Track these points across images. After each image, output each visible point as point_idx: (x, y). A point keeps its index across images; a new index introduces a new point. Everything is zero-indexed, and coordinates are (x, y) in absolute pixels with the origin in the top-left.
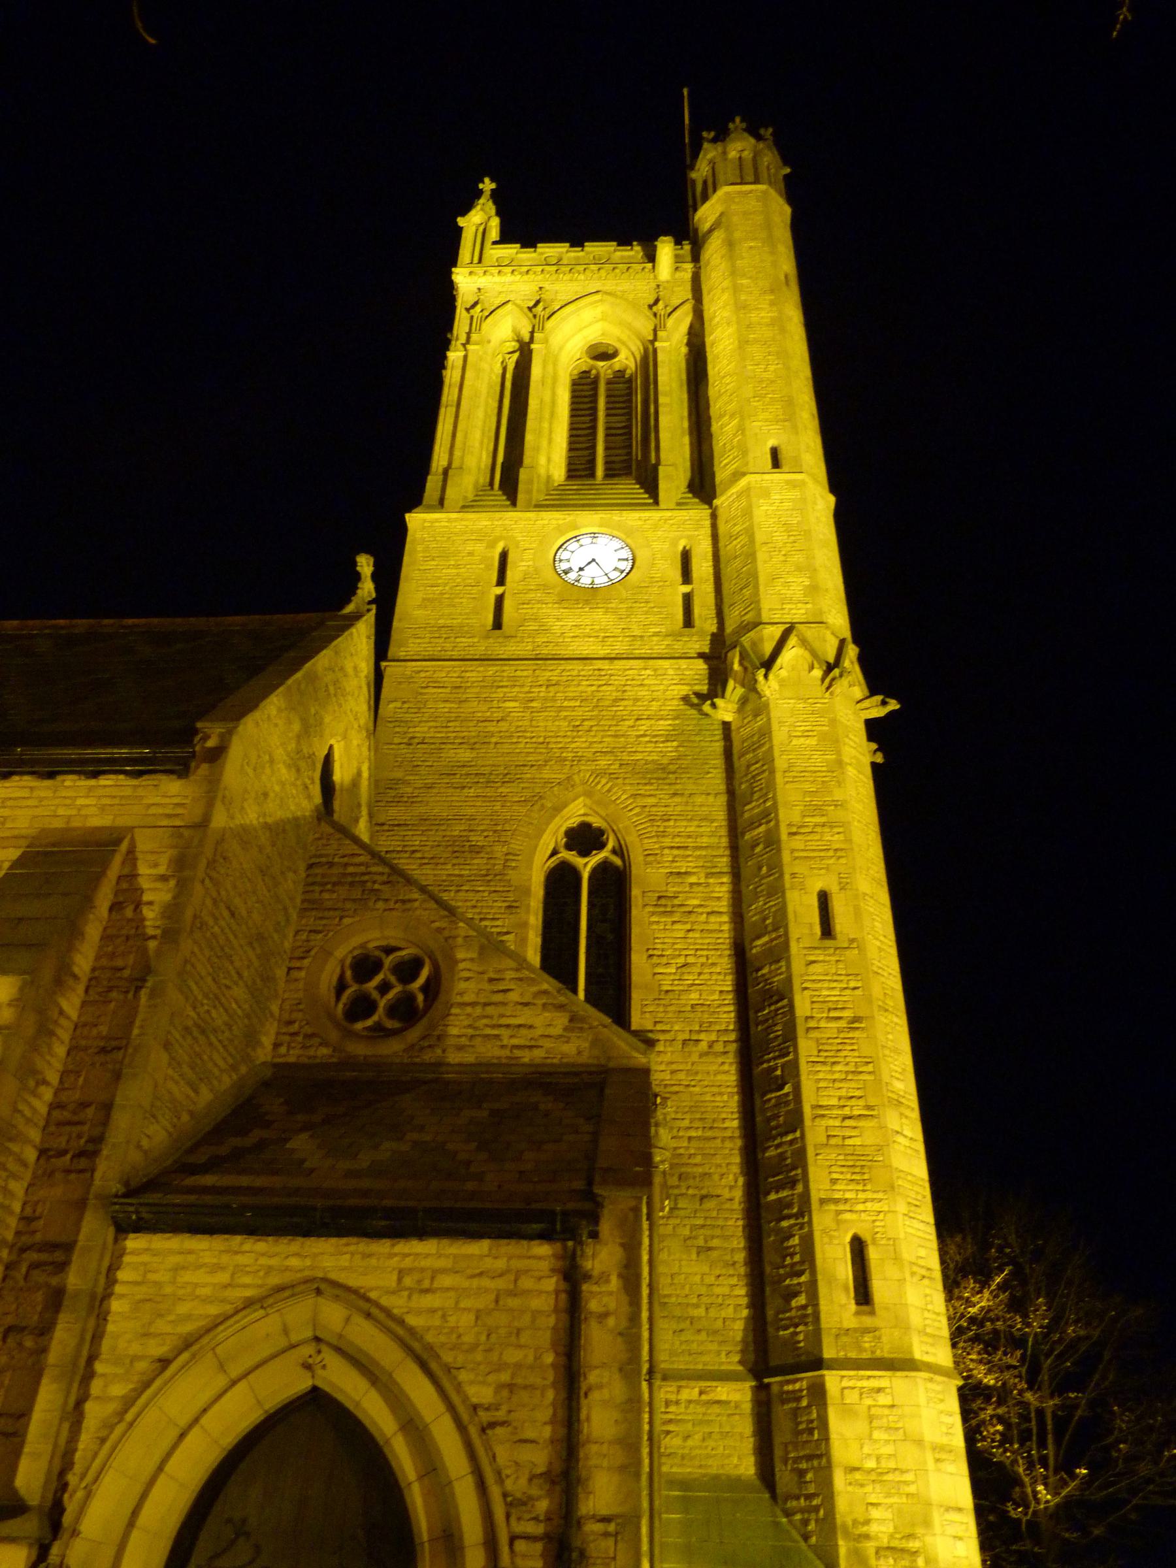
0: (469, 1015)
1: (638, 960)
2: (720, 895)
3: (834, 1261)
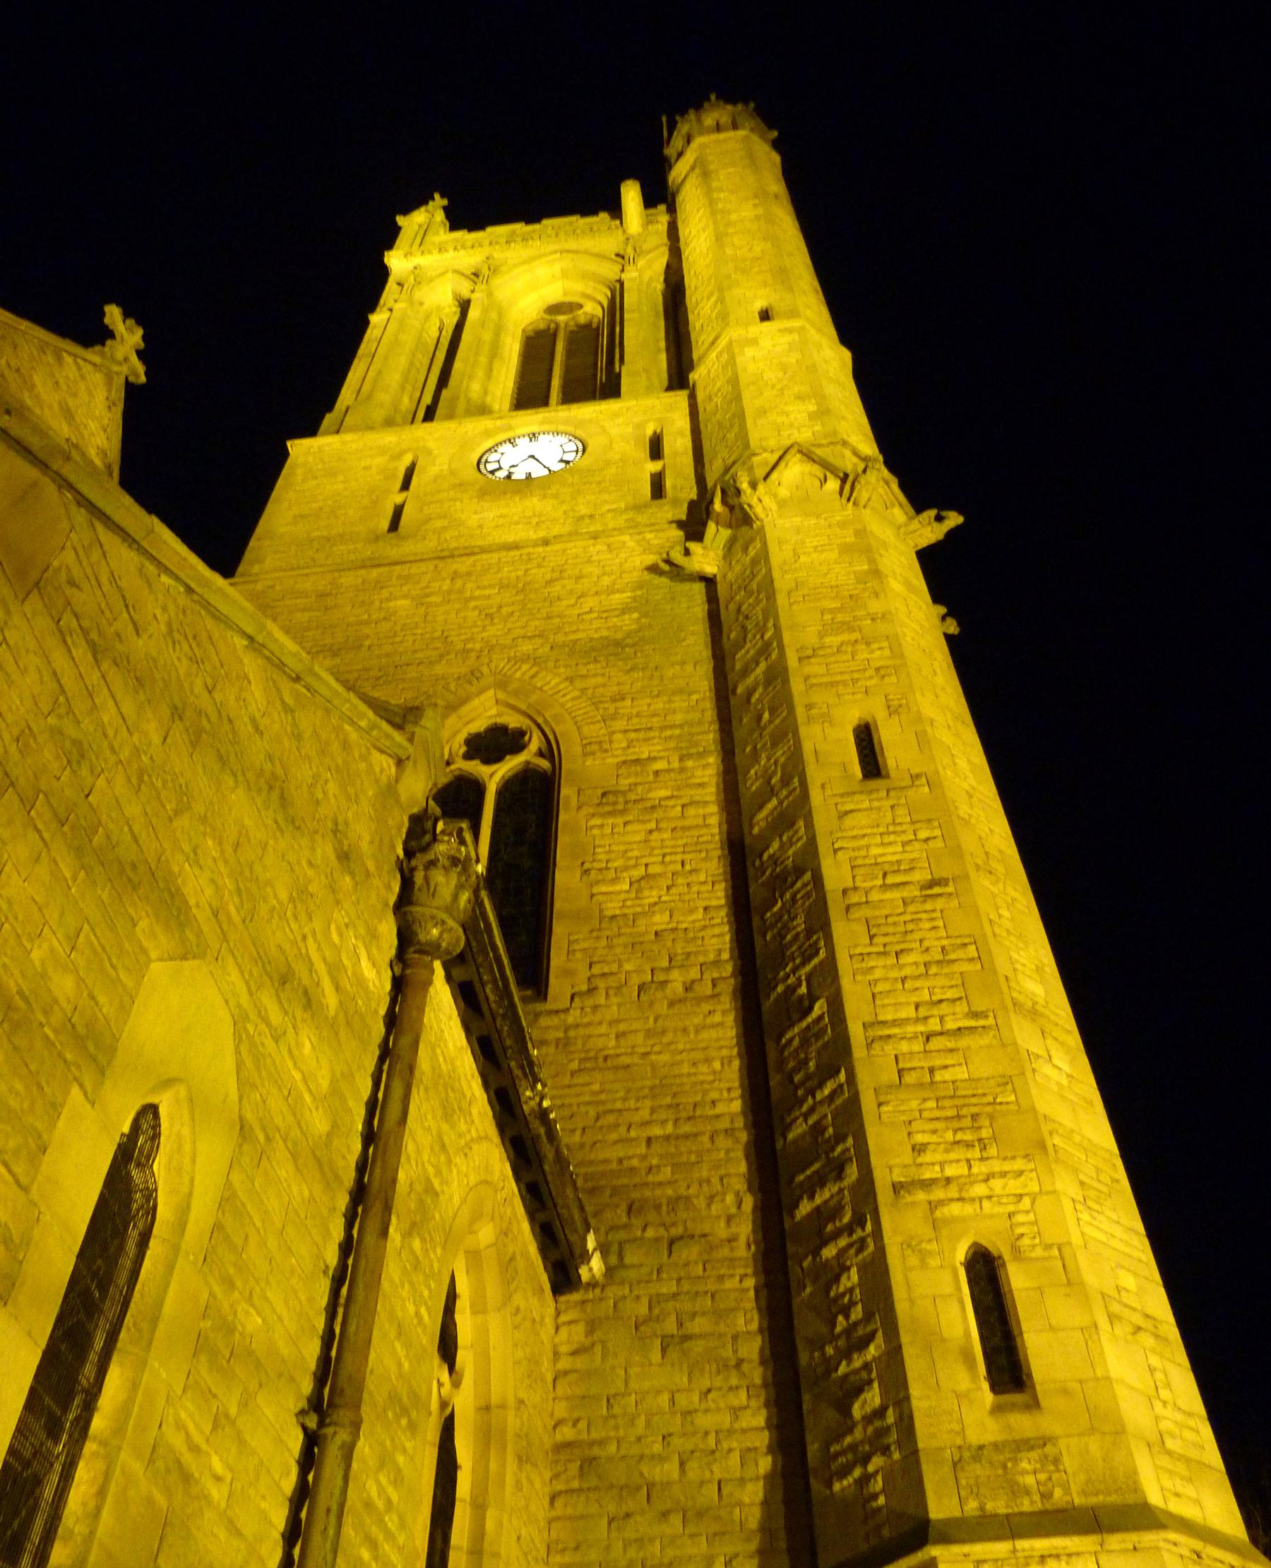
1: (566, 879)
3: (934, 1301)
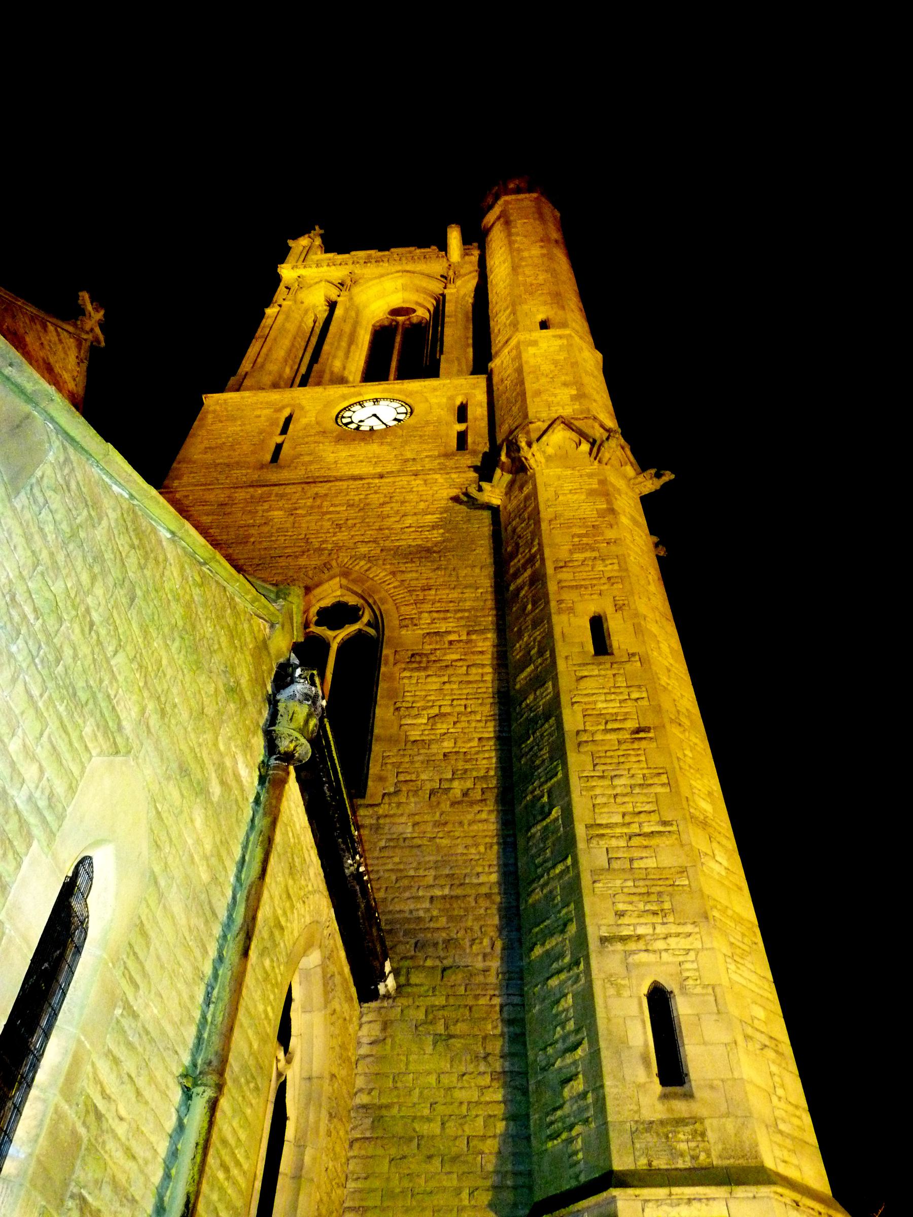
2: (484, 649)
3: (626, 1025)
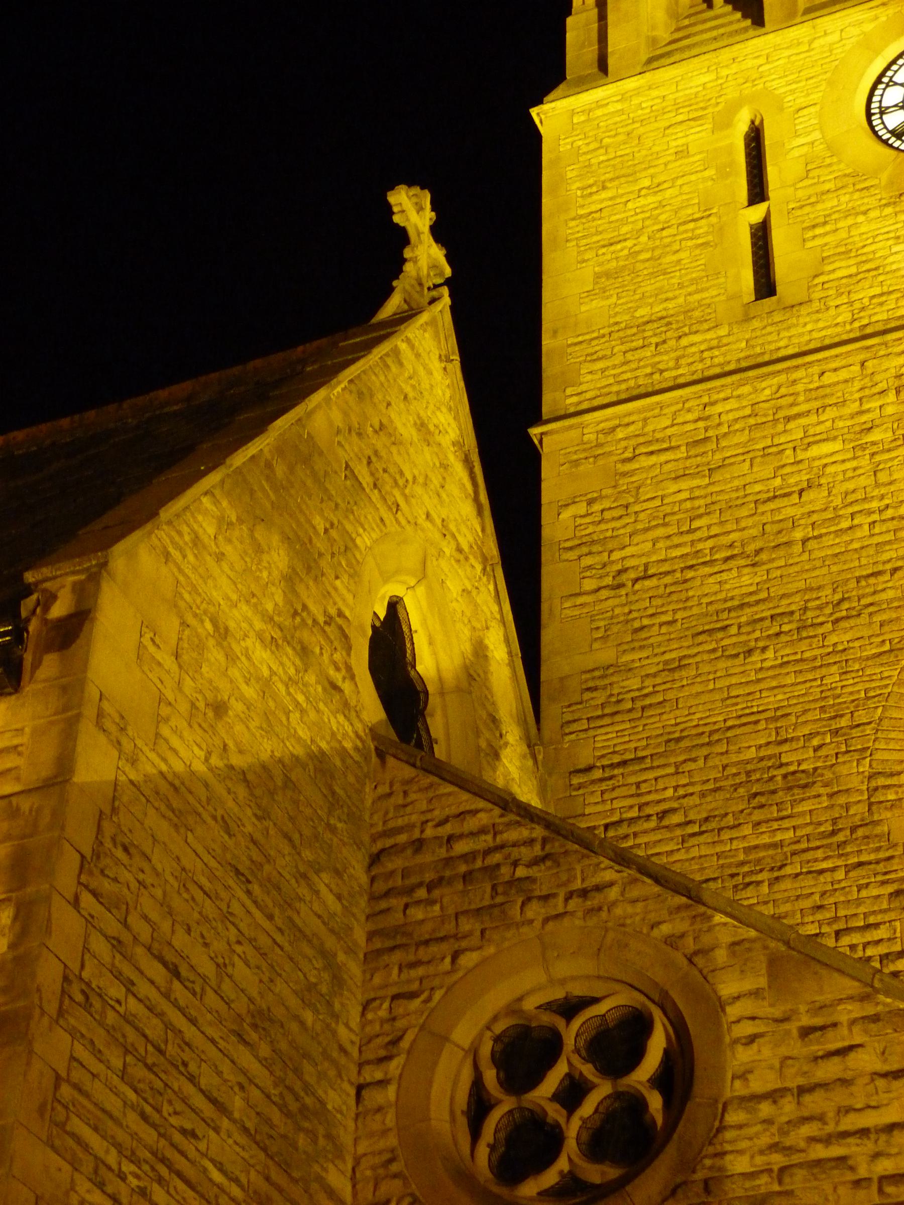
0: (768, 1122)
